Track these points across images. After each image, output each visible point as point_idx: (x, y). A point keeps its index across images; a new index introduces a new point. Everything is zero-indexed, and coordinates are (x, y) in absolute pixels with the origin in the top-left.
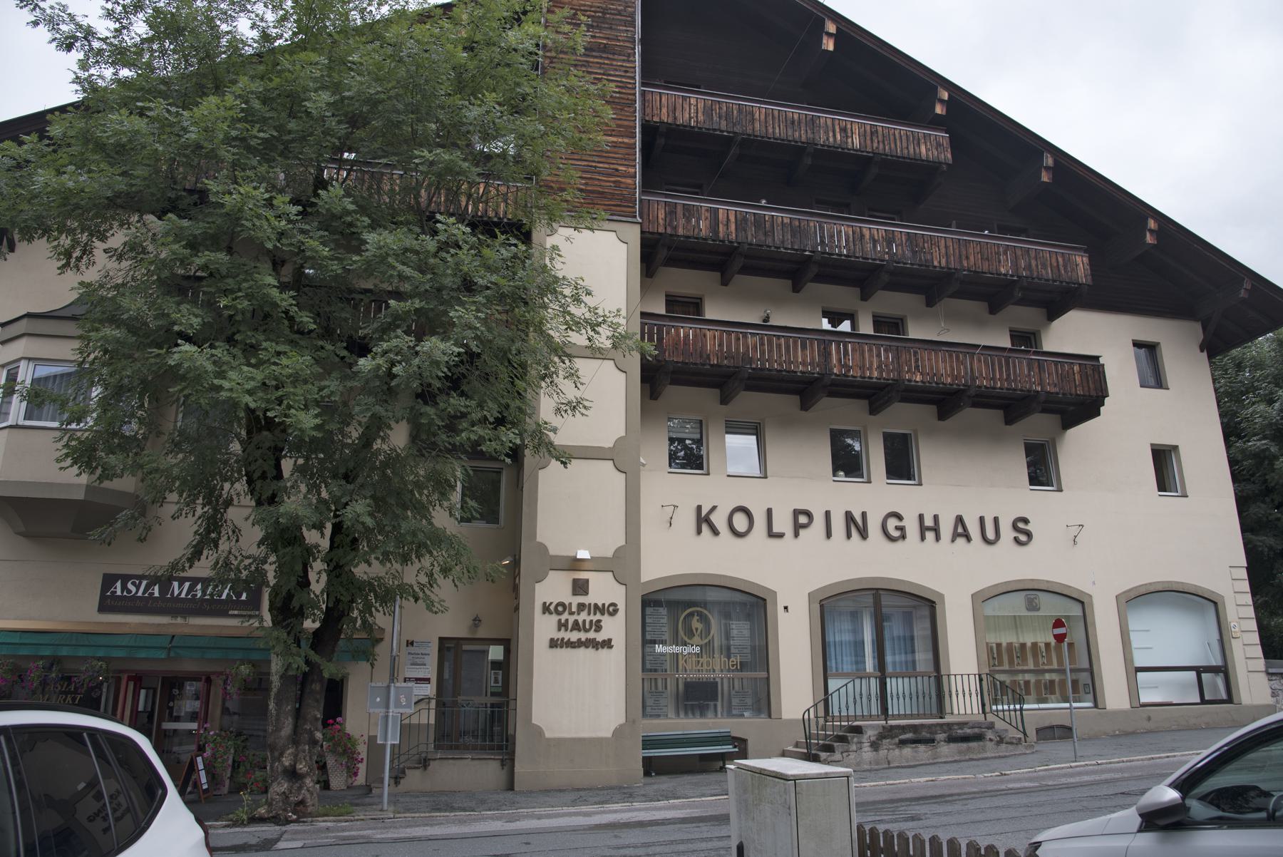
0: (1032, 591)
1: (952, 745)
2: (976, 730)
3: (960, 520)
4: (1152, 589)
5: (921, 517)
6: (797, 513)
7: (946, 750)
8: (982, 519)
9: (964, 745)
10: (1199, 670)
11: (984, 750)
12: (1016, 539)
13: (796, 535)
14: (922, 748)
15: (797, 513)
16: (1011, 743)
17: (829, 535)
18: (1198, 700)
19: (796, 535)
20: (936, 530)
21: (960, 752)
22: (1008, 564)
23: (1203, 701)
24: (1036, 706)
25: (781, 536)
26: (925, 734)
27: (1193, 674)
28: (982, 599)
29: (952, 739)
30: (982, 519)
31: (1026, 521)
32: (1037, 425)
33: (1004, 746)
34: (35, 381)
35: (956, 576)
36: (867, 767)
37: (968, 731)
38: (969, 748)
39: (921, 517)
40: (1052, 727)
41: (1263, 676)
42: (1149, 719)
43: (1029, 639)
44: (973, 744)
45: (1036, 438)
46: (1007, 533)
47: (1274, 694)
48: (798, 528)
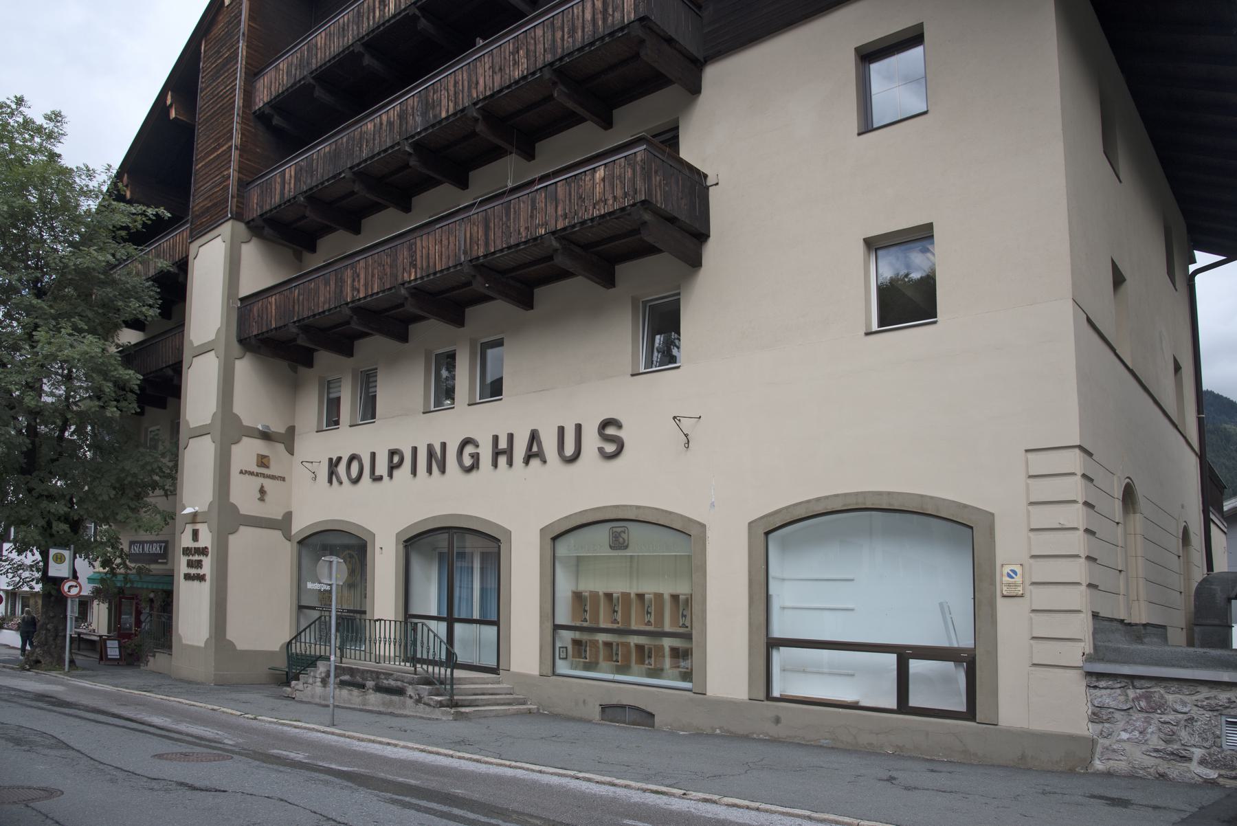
0: (617, 525)
1: (379, 695)
2: (399, 683)
3: (534, 436)
4: (820, 508)
5: (496, 439)
6: (392, 453)
7: (374, 699)
8: (561, 430)
9: (387, 697)
10: (904, 654)
11: (404, 706)
12: (601, 450)
13: (391, 475)
14: (356, 692)
15: (392, 453)
16: (429, 705)
17: (341, 483)
18: (892, 703)
19: (391, 475)
20: (509, 452)
21: (384, 704)
22: (593, 487)
23: (903, 706)
24: (610, 677)
25: (380, 478)
26: (359, 679)
27: (892, 659)
28: (556, 536)
29: (379, 689)
30: (561, 430)
31: (618, 425)
32: (640, 277)
33: (421, 706)
34: (639, 256)
35: (520, 506)
36: (317, 700)
37: (393, 683)
38: (391, 701)
39: (496, 439)
40: (623, 707)
41: (1076, 676)
42: (777, 720)
43: (649, 588)
44: (395, 698)
45: (656, 294)
46: (591, 441)
47: (1095, 718)
48: (392, 468)
